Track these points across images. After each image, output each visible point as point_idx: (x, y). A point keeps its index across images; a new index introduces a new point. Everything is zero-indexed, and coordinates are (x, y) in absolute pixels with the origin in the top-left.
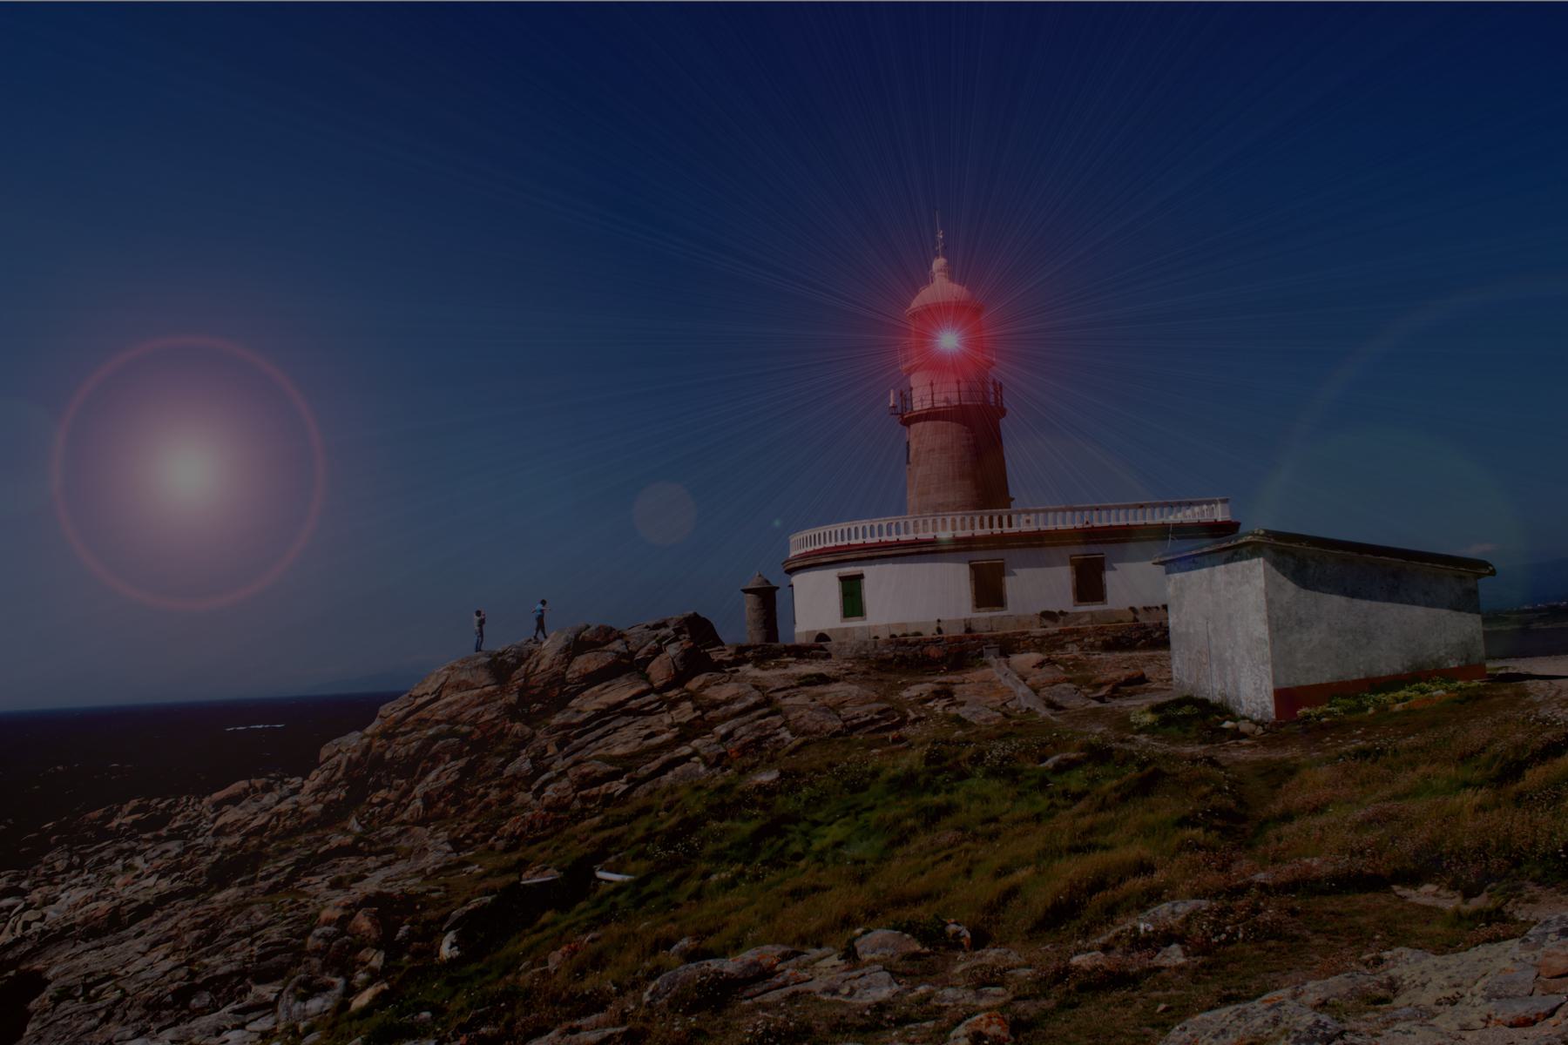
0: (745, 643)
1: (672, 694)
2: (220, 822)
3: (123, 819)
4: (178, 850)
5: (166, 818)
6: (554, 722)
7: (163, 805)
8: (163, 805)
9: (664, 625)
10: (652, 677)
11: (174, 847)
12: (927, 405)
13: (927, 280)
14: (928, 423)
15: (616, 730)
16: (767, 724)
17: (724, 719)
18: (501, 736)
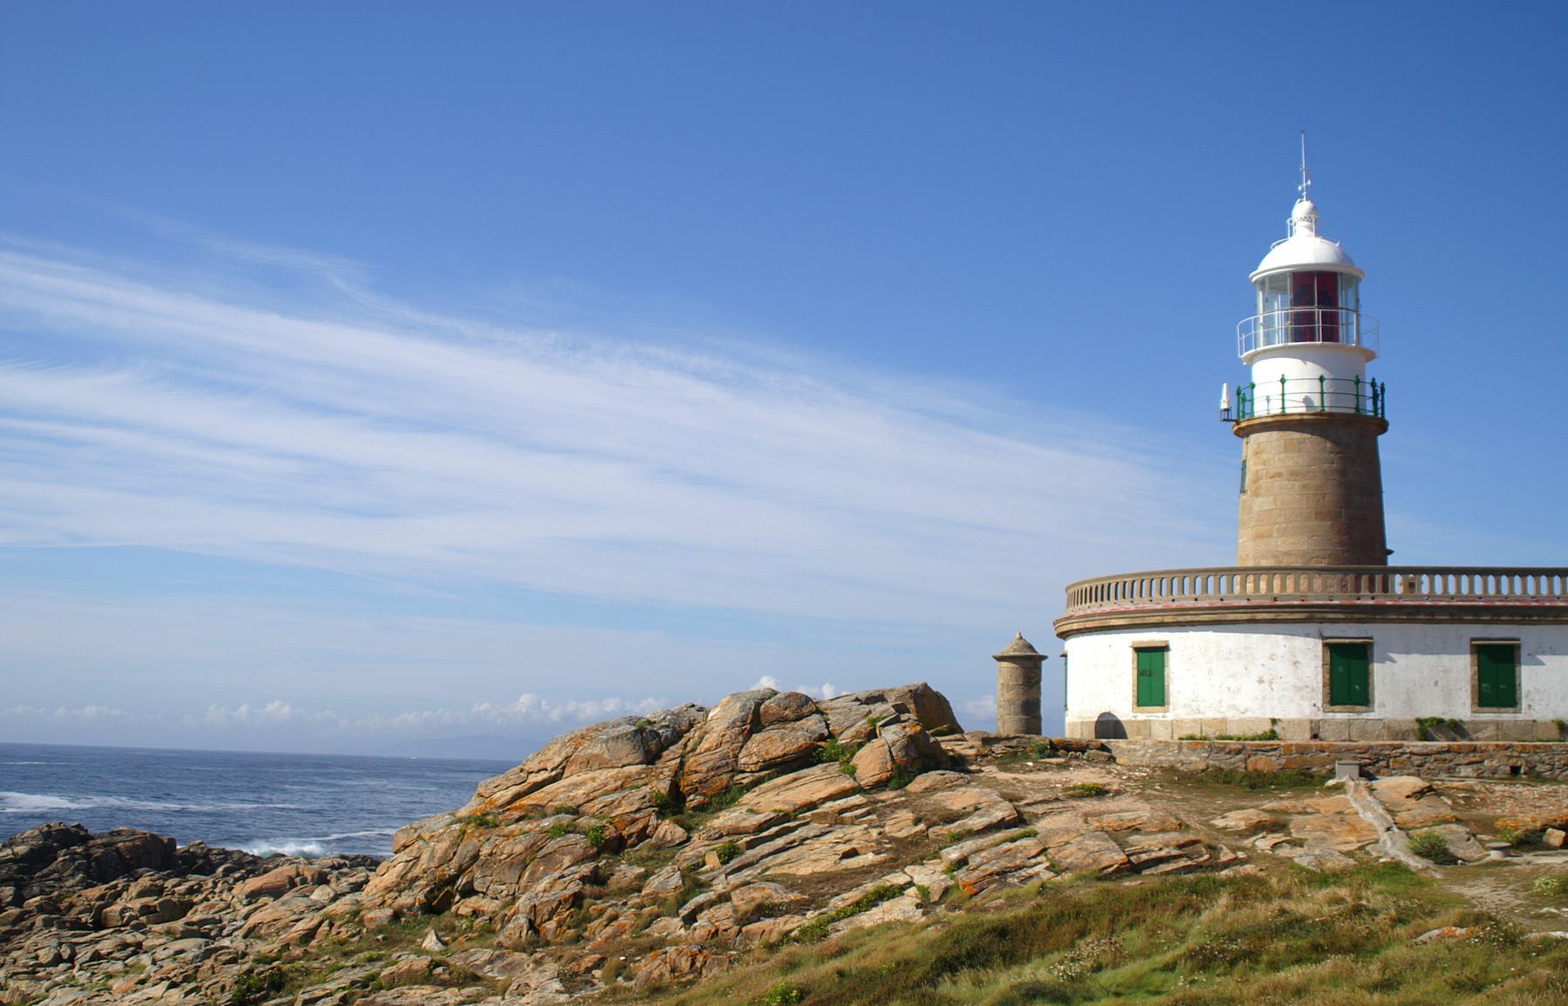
0: (993, 733)
1: (887, 796)
2: (252, 921)
3: (130, 901)
4: (196, 951)
5: (184, 908)
6: (717, 823)
7: (182, 888)
8: (182, 888)
9: (880, 698)
10: (858, 773)
11: (192, 946)
12: (1276, 409)
13: (1281, 232)
14: (1275, 434)
15: (803, 841)
16: (1018, 850)
17: (958, 838)
18: (643, 835)
